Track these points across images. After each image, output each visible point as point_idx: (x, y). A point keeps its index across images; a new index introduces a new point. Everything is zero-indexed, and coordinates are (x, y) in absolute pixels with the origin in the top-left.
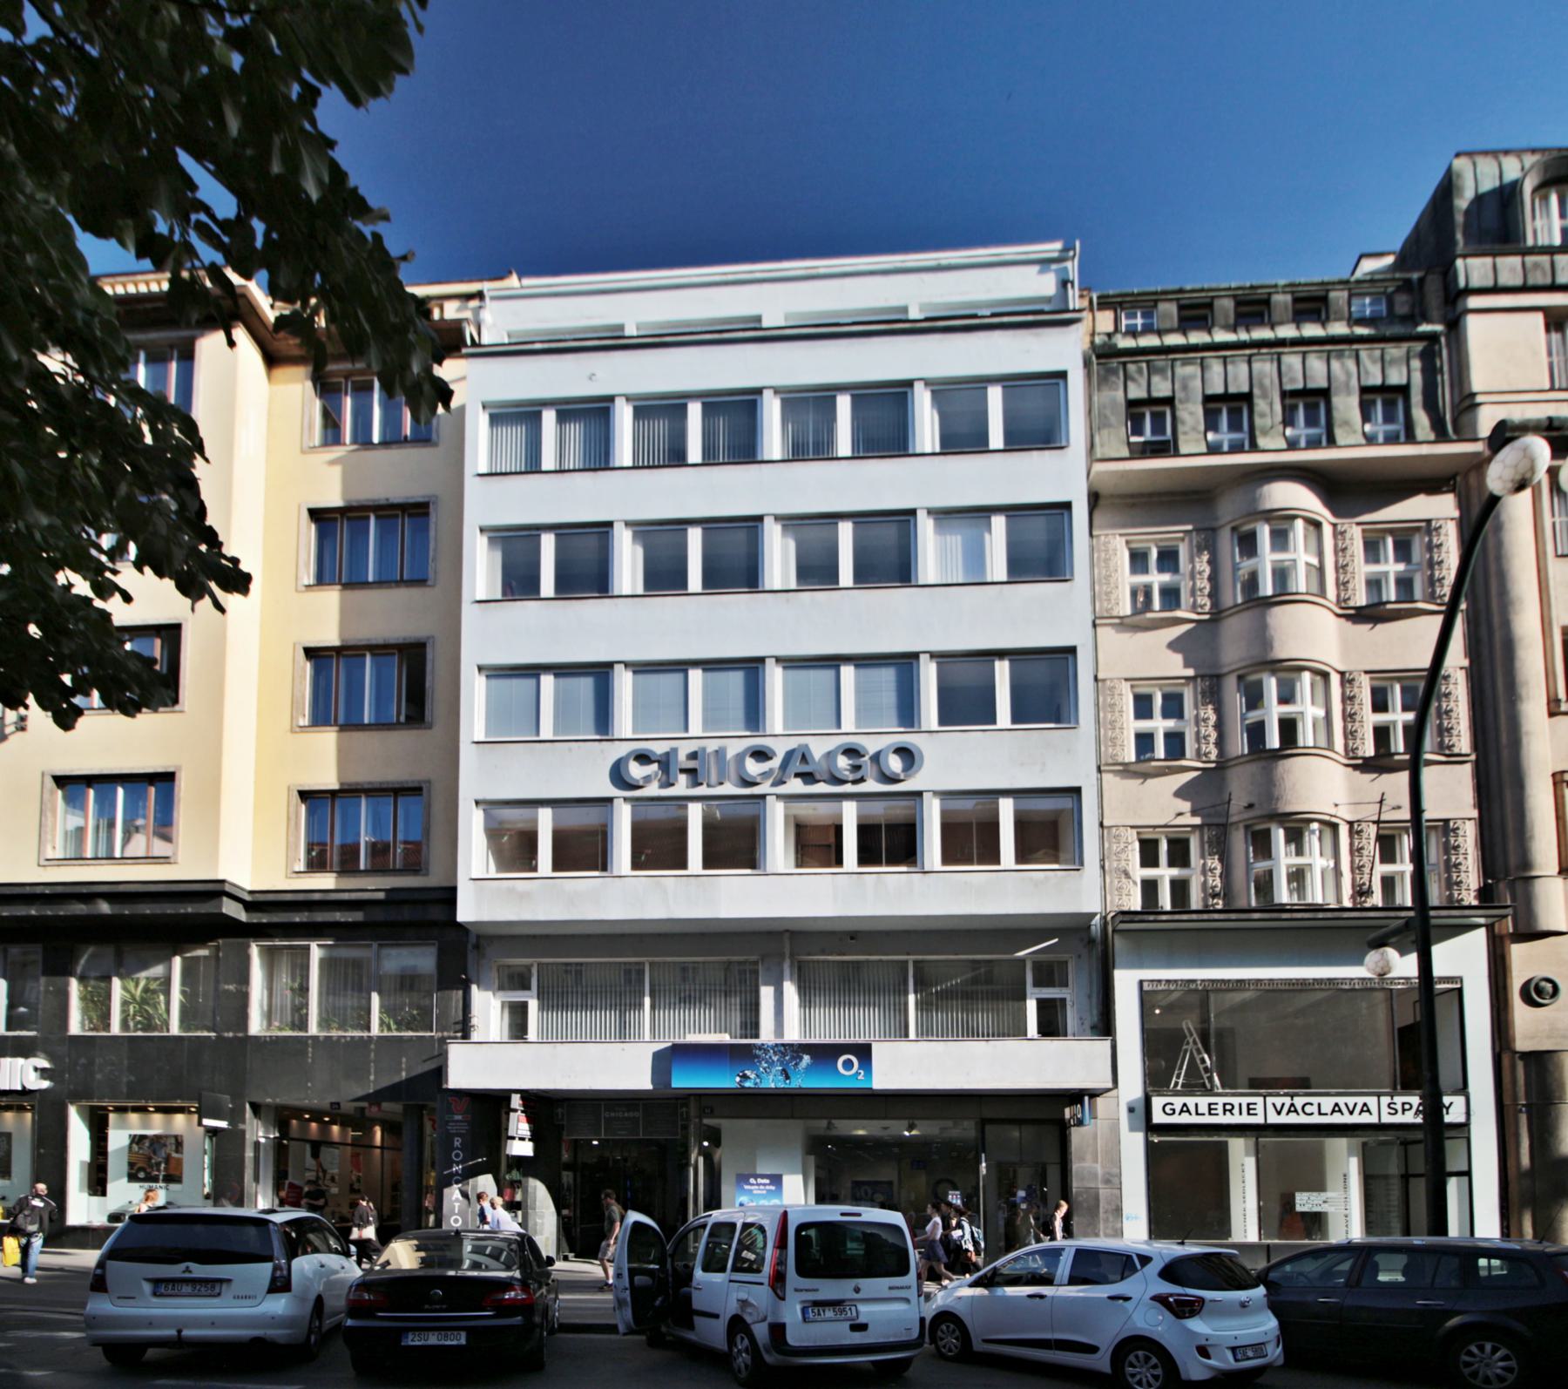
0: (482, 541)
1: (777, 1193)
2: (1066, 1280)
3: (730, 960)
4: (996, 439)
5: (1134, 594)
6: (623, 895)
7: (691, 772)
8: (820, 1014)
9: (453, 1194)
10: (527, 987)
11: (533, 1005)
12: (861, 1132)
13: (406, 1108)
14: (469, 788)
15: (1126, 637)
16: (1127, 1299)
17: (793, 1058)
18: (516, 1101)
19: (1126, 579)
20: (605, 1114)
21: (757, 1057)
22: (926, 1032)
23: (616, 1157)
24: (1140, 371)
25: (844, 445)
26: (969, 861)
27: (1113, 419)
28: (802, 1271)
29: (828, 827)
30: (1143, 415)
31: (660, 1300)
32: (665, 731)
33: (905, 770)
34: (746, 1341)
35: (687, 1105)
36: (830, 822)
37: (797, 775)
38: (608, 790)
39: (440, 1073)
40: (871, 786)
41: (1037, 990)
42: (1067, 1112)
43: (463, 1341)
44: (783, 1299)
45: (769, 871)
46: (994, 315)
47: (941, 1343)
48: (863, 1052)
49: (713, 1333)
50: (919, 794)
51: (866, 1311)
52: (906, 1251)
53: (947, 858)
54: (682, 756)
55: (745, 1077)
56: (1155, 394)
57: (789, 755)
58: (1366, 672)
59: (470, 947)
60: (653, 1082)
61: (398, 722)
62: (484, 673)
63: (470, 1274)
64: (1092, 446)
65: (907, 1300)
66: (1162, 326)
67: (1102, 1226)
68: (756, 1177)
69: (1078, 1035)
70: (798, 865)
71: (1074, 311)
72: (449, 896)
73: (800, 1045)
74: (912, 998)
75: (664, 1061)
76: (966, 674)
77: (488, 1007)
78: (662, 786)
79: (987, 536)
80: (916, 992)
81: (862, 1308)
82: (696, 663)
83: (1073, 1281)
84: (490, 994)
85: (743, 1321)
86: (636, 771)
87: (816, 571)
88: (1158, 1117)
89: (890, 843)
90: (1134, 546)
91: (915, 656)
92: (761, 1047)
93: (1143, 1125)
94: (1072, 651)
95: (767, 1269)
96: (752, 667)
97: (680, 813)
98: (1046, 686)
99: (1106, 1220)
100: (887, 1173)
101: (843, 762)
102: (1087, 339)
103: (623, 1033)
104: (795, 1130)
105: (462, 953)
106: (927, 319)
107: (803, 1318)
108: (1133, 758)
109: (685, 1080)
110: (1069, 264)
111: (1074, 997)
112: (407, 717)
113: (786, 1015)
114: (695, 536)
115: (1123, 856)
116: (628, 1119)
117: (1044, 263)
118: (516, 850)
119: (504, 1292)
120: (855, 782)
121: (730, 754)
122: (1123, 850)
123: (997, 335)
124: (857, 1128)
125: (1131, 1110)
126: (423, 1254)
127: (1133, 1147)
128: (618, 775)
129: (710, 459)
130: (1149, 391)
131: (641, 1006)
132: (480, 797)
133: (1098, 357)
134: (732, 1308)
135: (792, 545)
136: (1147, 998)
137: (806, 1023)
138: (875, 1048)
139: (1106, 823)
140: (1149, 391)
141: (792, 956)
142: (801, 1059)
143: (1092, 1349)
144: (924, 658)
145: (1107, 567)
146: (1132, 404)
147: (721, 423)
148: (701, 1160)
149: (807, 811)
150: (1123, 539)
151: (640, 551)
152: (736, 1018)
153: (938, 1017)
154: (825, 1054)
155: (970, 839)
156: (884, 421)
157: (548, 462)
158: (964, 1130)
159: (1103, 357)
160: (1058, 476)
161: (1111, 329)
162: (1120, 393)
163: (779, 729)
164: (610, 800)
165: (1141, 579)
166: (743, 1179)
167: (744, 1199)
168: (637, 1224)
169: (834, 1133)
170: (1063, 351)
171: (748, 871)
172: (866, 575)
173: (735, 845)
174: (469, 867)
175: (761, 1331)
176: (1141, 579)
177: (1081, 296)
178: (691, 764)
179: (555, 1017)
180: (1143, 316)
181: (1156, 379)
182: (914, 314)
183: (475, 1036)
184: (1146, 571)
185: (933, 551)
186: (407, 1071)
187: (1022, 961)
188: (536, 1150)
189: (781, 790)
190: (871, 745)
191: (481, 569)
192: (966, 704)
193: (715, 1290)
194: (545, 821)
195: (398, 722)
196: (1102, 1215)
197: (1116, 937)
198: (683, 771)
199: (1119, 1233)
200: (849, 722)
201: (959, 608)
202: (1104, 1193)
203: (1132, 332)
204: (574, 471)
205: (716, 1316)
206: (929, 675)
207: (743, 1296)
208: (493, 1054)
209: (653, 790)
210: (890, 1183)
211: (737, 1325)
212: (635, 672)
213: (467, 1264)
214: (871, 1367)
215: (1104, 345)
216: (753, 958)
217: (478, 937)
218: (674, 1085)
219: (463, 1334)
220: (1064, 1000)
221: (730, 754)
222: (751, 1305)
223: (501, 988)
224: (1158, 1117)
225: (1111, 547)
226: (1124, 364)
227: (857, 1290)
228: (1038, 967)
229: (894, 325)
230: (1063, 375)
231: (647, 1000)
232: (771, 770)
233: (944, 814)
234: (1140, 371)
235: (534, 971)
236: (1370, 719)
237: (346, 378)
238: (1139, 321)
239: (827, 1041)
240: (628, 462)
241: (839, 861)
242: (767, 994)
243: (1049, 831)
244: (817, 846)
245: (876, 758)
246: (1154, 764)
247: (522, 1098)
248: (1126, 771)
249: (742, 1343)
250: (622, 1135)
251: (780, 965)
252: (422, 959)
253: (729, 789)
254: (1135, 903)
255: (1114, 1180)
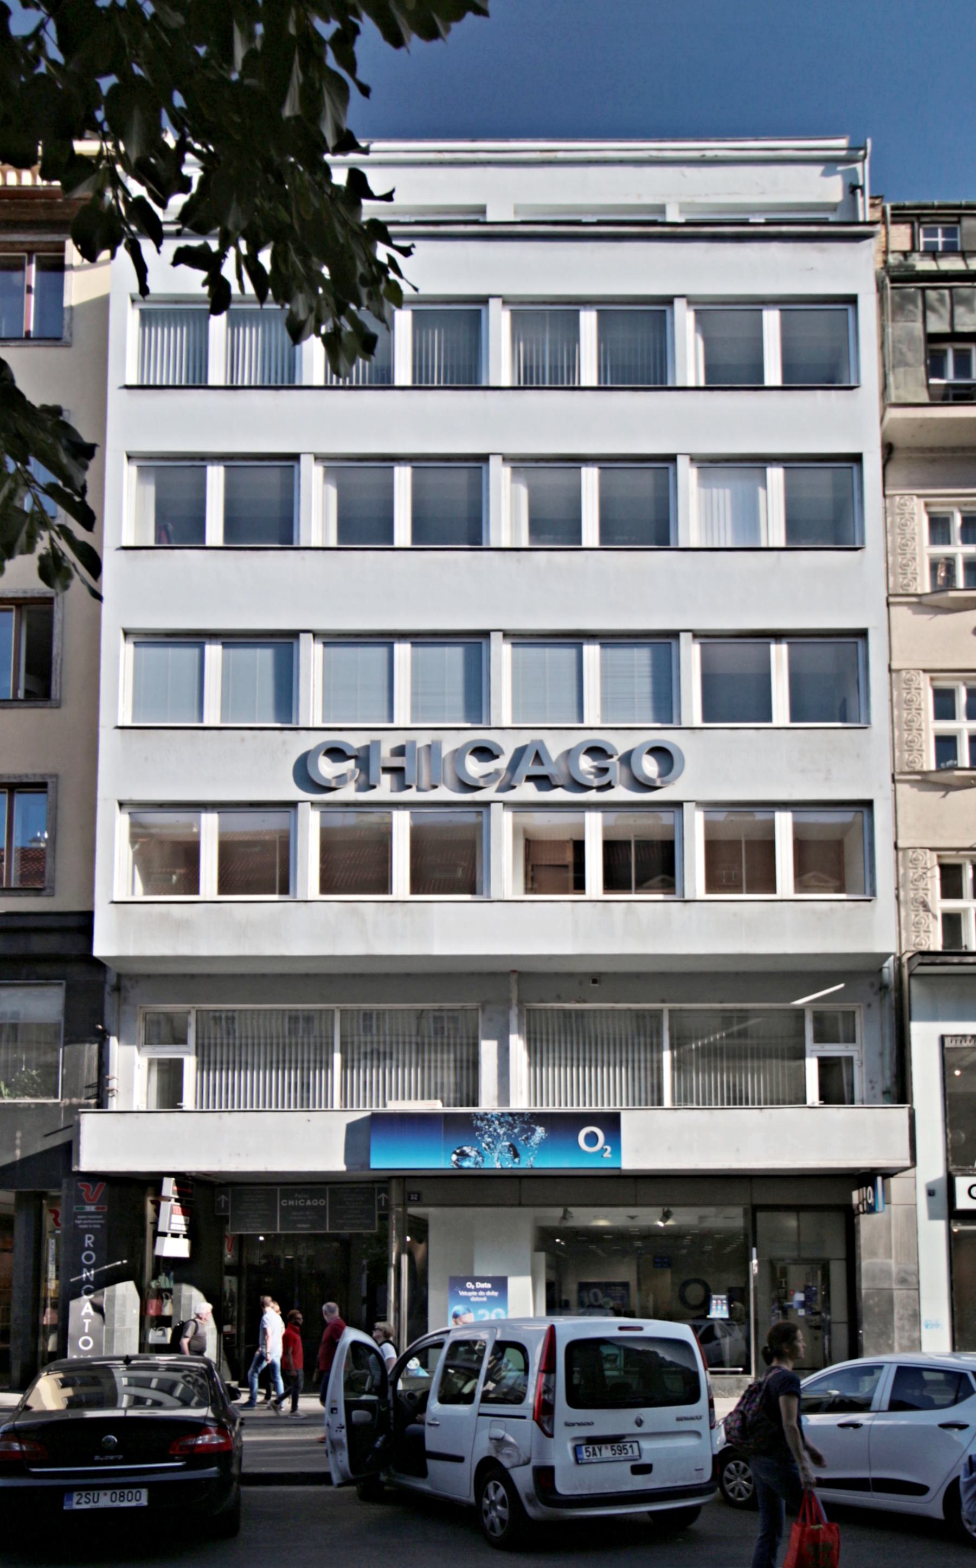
0: (130, 471)
1: (501, 1301)
2: (885, 1406)
3: (446, 1007)
4: (773, 374)
5: (934, 567)
6: (309, 925)
7: (397, 771)
8: (554, 1075)
9: (82, 1308)
10: (182, 1040)
11: (190, 1063)
12: (602, 1223)
13: (19, 1196)
14: (109, 789)
15: (925, 620)
16: (962, 1427)
17: (523, 1131)
18: (169, 1187)
19: (925, 549)
20: (282, 1203)
21: (478, 1129)
22: (683, 1099)
23: (304, 1253)
24: (941, 300)
25: (589, 374)
26: (737, 889)
27: (910, 357)
28: (574, 1400)
29: (563, 843)
30: (945, 352)
31: (387, 1436)
32: (634, 722)
33: (661, 775)
34: (502, 1491)
35: (386, 1191)
36: (566, 837)
37: (529, 778)
38: (293, 792)
39: (69, 1150)
40: (621, 793)
41: (818, 1046)
42: (856, 1196)
43: (144, 1502)
44: (551, 1436)
45: (494, 896)
46: (767, 224)
47: (728, 1486)
48: (611, 1123)
49: (456, 1482)
50: (679, 805)
51: (650, 1449)
52: (696, 1375)
53: (713, 884)
54: (385, 751)
55: (463, 1155)
56: (959, 329)
57: (520, 753)
58: (925, 671)
59: (108, 988)
60: (346, 1162)
61: (16, 699)
62: (132, 639)
63: (132, 1413)
64: (885, 388)
65: (697, 1434)
66: (966, 248)
67: (896, 1335)
68: (474, 1280)
69: (869, 1102)
70: (528, 890)
71: (865, 223)
72: (83, 924)
73: (533, 1115)
74: (667, 1056)
75: (360, 1136)
76: (735, 657)
77: (131, 1066)
78: (360, 789)
79: (761, 491)
80: (672, 1048)
81: (646, 1445)
82: (403, 636)
83: (896, 1405)
84: (135, 1048)
85: (499, 1464)
86: (327, 769)
87: (554, 527)
88: (963, 1202)
89: (643, 864)
90: (933, 509)
91: (674, 634)
92: (483, 1117)
93: (944, 1209)
94: (863, 634)
95: (531, 1398)
96: (284, 642)
97: (386, 820)
98: (832, 675)
99: (902, 1329)
100: (625, 1272)
101: (586, 764)
102: (880, 258)
103: (305, 1100)
104: (524, 1222)
105: (96, 995)
106: (687, 224)
107: (578, 1459)
108: (933, 767)
109: (387, 1159)
110: (858, 166)
111: (863, 1054)
112: (27, 692)
113: (512, 1077)
114: (403, 476)
115: (921, 884)
116: (312, 1208)
117: (829, 163)
118: (170, 865)
119: (197, 1435)
120: (601, 788)
121: (446, 750)
122: (922, 877)
123: (775, 248)
124: (596, 1217)
125: (931, 1193)
126: (69, 1392)
127: (933, 1237)
128: (304, 774)
129: (421, 384)
130: (952, 324)
131: (328, 1065)
132: (125, 797)
133: (893, 280)
134: (483, 1448)
135: (524, 492)
136: (949, 1054)
137: (536, 1089)
138: (625, 1118)
139: (900, 844)
140: (952, 324)
141: (520, 1002)
142: (533, 1131)
143: (921, 1490)
144: (685, 638)
145: (903, 534)
146: (932, 338)
147: (436, 337)
148: (405, 1259)
149: (540, 821)
150: (922, 501)
151: (333, 492)
152: (449, 1078)
153: (697, 1080)
154: (563, 1125)
155: (740, 862)
156: (637, 348)
157: (217, 374)
158: (731, 1218)
159: (898, 279)
160: (847, 421)
161: (907, 246)
162: (919, 325)
163: (507, 721)
164: (293, 805)
165: (942, 550)
166: (457, 1283)
167: (458, 1308)
168: (355, 1345)
169: (571, 1223)
170: (850, 270)
171: (468, 897)
172: (613, 536)
173: (450, 865)
174: (110, 887)
175: (523, 1478)
176: (942, 550)
177: (872, 206)
178: (397, 762)
179: (217, 1077)
180: (945, 234)
181: (960, 310)
182: (673, 215)
183: (114, 1104)
184: (947, 541)
185: (697, 506)
186: (23, 1147)
187: (799, 1013)
188: (193, 1249)
189: (510, 796)
190: (620, 743)
191: (126, 506)
192: (734, 699)
193: (459, 1429)
194: (209, 829)
195: (16, 699)
196: (897, 1323)
197: (914, 982)
198: (386, 770)
199: (916, 1344)
200: (592, 717)
201: (728, 578)
202: (899, 1294)
203: (932, 253)
204: (250, 388)
205: (460, 1459)
206: (691, 656)
207: (500, 1433)
208: (140, 1124)
209: (349, 793)
210: (625, 1285)
211: (490, 1470)
212: (325, 644)
213: (125, 1401)
214: (648, 1518)
215: (900, 266)
216: (470, 1005)
217: (119, 976)
218: (373, 1165)
219: (144, 1492)
220: (850, 1060)
221: (446, 750)
222: (509, 1444)
223: (148, 1042)
224: (963, 1202)
225: (907, 510)
226: (923, 289)
227: (639, 1423)
228: (819, 1018)
229: (647, 228)
230: (852, 300)
231: (337, 1058)
232: (497, 772)
233: (709, 827)
234: (941, 300)
235: (192, 1019)
236: (933, 727)
237: (30, 253)
238: (940, 239)
239: (563, 1109)
240: (506, 379)
241: (579, 885)
242: (488, 1049)
243: (835, 853)
244: (551, 868)
245: (627, 759)
246: (957, 773)
247: (177, 1183)
248: (925, 781)
249: (496, 1493)
250: (303, 1229)
251: (506, 1014)
252: (42, 1004)
253: (444, 793)
254: (936, 942)
255: (911, 1280)
